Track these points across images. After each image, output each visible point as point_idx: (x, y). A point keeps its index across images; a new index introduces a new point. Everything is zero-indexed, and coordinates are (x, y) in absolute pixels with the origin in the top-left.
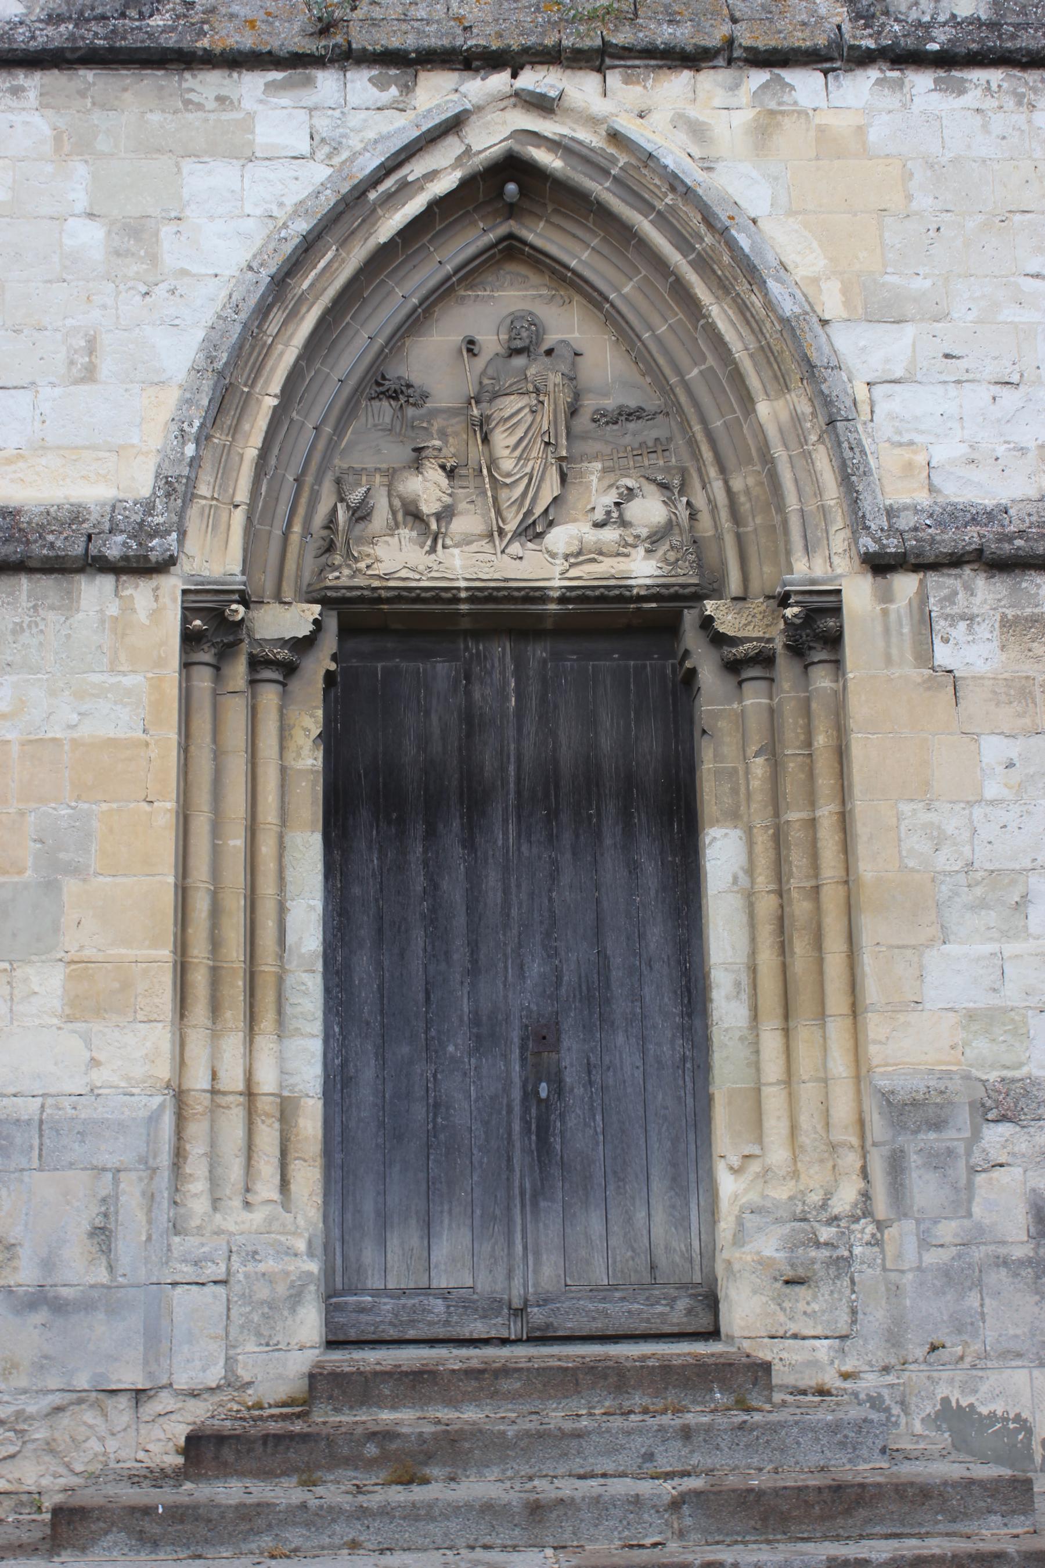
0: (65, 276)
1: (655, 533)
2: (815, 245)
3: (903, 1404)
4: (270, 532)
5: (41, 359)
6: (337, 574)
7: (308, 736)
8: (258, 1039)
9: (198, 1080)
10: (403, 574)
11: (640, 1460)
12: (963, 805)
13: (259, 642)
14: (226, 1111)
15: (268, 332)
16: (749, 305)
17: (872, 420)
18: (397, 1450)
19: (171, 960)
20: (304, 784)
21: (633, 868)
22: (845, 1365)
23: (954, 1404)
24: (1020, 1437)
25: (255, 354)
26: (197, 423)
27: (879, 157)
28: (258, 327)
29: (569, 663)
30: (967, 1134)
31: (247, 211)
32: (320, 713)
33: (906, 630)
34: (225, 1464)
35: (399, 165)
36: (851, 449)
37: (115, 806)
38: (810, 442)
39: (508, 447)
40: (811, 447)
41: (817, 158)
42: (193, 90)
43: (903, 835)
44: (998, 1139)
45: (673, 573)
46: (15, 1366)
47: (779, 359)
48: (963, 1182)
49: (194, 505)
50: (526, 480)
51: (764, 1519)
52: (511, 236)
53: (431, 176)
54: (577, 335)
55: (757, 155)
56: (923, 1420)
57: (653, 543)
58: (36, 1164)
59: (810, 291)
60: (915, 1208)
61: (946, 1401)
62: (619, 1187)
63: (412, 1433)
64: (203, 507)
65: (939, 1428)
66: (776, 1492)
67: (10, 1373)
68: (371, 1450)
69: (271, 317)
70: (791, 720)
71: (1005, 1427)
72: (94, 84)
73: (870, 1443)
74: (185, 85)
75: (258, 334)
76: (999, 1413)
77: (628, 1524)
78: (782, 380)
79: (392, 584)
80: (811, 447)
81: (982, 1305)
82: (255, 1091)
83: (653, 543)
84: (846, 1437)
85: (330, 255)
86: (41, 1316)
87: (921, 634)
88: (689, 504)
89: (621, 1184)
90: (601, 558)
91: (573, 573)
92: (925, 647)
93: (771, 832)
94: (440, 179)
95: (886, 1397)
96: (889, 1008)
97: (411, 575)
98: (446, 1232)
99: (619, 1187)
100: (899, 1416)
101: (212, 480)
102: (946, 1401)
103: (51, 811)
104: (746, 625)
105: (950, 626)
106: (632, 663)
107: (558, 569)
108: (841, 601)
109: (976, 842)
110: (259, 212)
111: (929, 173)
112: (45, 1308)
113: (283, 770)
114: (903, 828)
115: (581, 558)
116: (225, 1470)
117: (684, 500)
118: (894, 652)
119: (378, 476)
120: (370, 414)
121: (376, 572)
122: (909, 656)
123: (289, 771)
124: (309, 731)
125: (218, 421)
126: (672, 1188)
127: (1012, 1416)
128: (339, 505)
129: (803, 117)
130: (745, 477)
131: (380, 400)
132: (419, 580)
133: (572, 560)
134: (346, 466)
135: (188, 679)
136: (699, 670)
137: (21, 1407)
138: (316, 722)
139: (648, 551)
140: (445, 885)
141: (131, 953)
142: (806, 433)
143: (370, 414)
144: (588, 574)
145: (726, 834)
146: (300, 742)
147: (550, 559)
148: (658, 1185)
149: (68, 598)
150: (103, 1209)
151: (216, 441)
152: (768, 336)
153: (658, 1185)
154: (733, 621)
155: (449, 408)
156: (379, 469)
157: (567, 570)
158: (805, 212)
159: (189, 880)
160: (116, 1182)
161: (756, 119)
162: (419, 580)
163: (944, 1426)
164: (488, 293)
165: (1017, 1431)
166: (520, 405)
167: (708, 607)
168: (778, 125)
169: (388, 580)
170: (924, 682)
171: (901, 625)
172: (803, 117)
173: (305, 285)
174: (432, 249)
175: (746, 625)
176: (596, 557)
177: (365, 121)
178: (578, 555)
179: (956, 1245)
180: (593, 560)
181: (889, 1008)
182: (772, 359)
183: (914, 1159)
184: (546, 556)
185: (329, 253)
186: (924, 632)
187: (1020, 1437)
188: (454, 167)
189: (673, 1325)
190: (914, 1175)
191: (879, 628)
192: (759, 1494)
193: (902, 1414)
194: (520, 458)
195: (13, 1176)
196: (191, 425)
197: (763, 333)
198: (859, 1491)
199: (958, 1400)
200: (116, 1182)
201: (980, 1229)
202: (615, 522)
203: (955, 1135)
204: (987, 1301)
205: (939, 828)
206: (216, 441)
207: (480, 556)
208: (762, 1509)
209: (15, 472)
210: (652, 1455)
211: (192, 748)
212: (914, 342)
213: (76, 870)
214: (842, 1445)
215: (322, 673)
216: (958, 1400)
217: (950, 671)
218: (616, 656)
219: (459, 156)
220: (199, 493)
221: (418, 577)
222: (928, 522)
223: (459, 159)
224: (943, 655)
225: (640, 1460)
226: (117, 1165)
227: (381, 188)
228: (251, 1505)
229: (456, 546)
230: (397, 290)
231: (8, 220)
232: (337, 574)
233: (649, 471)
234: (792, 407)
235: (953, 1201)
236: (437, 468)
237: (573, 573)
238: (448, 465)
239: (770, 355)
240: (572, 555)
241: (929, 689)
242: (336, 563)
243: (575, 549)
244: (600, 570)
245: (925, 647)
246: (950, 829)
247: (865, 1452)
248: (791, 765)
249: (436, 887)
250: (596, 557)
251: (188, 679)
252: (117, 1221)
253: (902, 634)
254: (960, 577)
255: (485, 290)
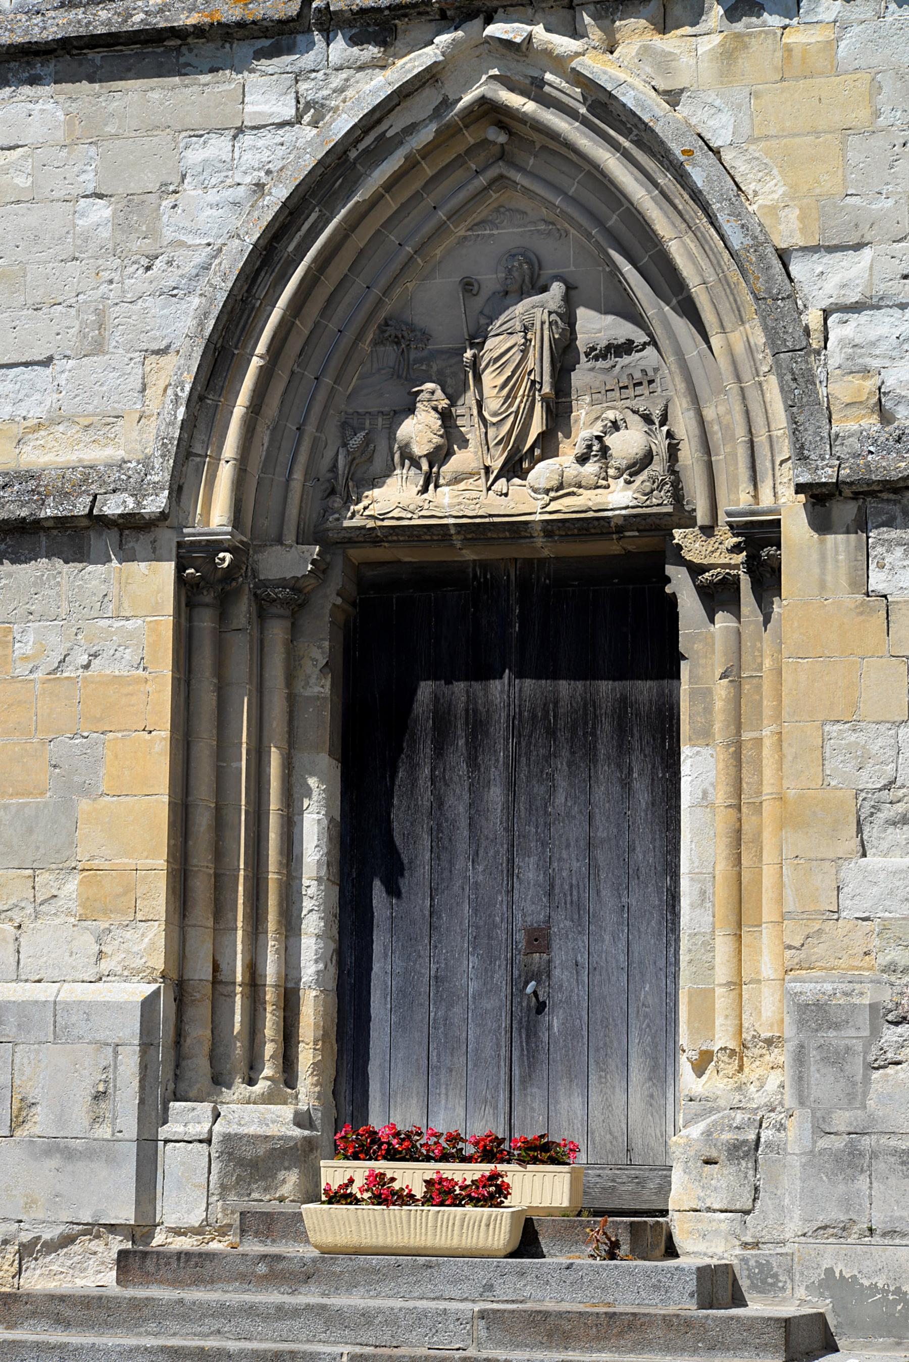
0: (77, 255)
1: (634, 465)
2: (775, 171)
3: (790, 1271)
4: (272, 480)
5: (58, 334)
6: (337, 516)
7: (315, 666)
8: (192, 933)
9: (201, 971)
10: (395, 514)
11: (481, 1290)
12: (888, 725)
13: (265, 584)
14: (228, 999)
15: (257, 296)
16: (709, 238)
17: (825, 348)
18: (282, 1270)
19: (165, 868)
20: (311, 710)
21: (626, 785)
22: (745, 1236)
23: (837, 1275)
24: (899, 1307)
25: (245, 317)
26: (188, 388)
27: (846, 72)
28: (247, 291)
29: (570, 589)
30: (867, 1033)
31: (238, 180)
32: (326, 644)
33: (841, 557)
34: (148, 1274)
35: (379, 121)
36: (795, 380)
37: (119, 735)
38: (761, 373)
39: (496, 387)
40: (762, 378)
41: (782, 79)
42: (189, 65)
43: (827, 755)
44: (895, 1039)
45: (648, 503)
46: (34, 1201)
47: (735, 292)
48: (859, 1078)
49: (190, 462)
50: (512, 418)
51: (550, 1336)
52: (502, 177)
53: (411, 129)
54: (572, 268)
55: (722, 83)
56: (807, 1287)
57: (631, 475)
58: (51, 1039)
59: (766, 222)
60: (812, 1099)
61: (830, 1271)
62: (601, 1077)
63: (295, 1257)
64: (197, 464)
65: (821, 1295)
66: (560, 1315)
67: (31, 1207)
68: (262, 1269)
69: (259, 281)
70: (749, 644)
71: (885, 1298)
72: (102, 67)
73: (680, 1288)
74: (182, 60)
75: (247, 298)
76: (880, 1285)
77: (437, 1331)
78: (737, 312)
79: (387, 523)
80: (762, 378)
81: (871, 1188)
82: (259, 983)
83: (631, 475)
84: (659, 1281)
85: (314, 216)
86: (54, 1162)
87: (856, 560)
88: (669, 435)
89: (603, 1074)
90: (581, 491)
91: (553, 506)
92: (860, 573)
93: (732, 749)
94: (419, 131)
95: (775, 1264)
96: (805, 916)
97: (403, 514)
98: (442, 1112)
99: (601, 1077)
100: (785, 1282)
101: (206, 439)
102: (830, 1271)
103: (67, 740)
104: (713, 552)
105: (887, 551)
106: (631, 587)
107: (540, 503)
108: (780, 532)
109: (900, 761)
110: (248, 179)
111: (899, 84)
112: (58, 1156)
113: (292, 699)
114: (828, 749)
115: (561, 492)
116: (148, 1279)
117: (665, 429)
118: (829, 578)
119: (380, 419)
120: (375, 360)
121: (371, 513)
122: (844, 582)
123: (297, 698)
124: (317, 661)
125: (211, 383)
126: (650, 1079)
127: (892, 1288)
128: (341, 450)
129: (771, 37)
130: (716, 407)
131: (385, 345)
132: (411, 519)
133: (552, 494)
134: (351, 411)
135: (190, 619)
136: (678, 595)
137: (39, 1234)
138: (323, 653)
139: (628, 483)
140: (450, 801)
141: (130, 862)
142: (758, 363)
143: (375, 360)
144: (566, 506)
145: (698, 752)
146: (308, 672)
147: (533, 494)
148: (637, 1075)
149: (80, 553)
150: (104, 1076)
151: (209, 402)
152: (725, 268)
153: (637, 1075)
154: (699, 549)
155: (450, 348)
156: (382, 412)
157: (548, 505)
158: (767, 137)
159: (190, 798)
160: (116, 1053)
161: (722, 45)
162: (411, 519)
163: (827, 1293)
164: (488, 232)
165: (896, 1302)
166: (508, 345)
167: (676, 535)
168: (746, 47)
169: (383, 520)
170: (857, 607)
171: (837, 553)
172: (771, 37)
173: (291, 248)
174: (425, 196)
175: (713, 552)
176: (575, 489)
177: (347, 80)
178: (560, 488)
179: (849, 1134)
180: (573, 494)
181: (805, 916)
182: (728, 291)
183: (813, 1055)
184: (530, 491)
185: (313, 214)
186: (860, 558)
187: (899, 1307)
188: (431, 118)
189: (645, 1202)
190: (813, 1069)
191: (815, 556)
192: (546, 1314)
193: (789, 1281)
194: (507, 397)
195: (32, 1047)
196: (182, 390)
197: (720, 266)
198: (631, 1318)
199: (841, 1271)
200: (116, 1053)
201: (872, 1118)
202: (595, 456)
203: (852, 1033)
204: (875, 1185)
205: (864, 747)
206: (209, 402)
207: (467, 494)
208: (548, 1327)
209: (37, 439)
210: (492, 1286)
211: (193, 682)
212: (872, 265)
213: (85, 790)
214: (656, 1288)
215: (329, 606)
216: (841, 1271)
217: (885, 596)
218: (616, 581)
219: (437, 106)
220: (194, 451)
221: (409, 515)
222: (872, 449)
223: (437, 110)
224: (878, 581)
225: (481, 1290)
226: (117, 1041)
227: (362, 146)
228: (141, 1299)
229: (448, 485)
230: (444, 218)
231: (29, 205)
232: (337, 516)
233: (634, 402)
234: (745, 339)
235: (848, 1094)
236: (430, 410)
237: (553, 506)
238: (440, 407)
239: (726, 287)
240: (551, 489)
241: (861, 613)
242: (336, 505)
243: (554, 483)
244: (578, 503)
245: (860, 573)
246: (874, 748)
247: (675, 1295)
248: (747, 687)
249: (441, 804)
250: (575, 489)
251: (190, 619)
252: (115, 1086)
253: (837, 561)
254: (900, 502)
255: (485, 230)
